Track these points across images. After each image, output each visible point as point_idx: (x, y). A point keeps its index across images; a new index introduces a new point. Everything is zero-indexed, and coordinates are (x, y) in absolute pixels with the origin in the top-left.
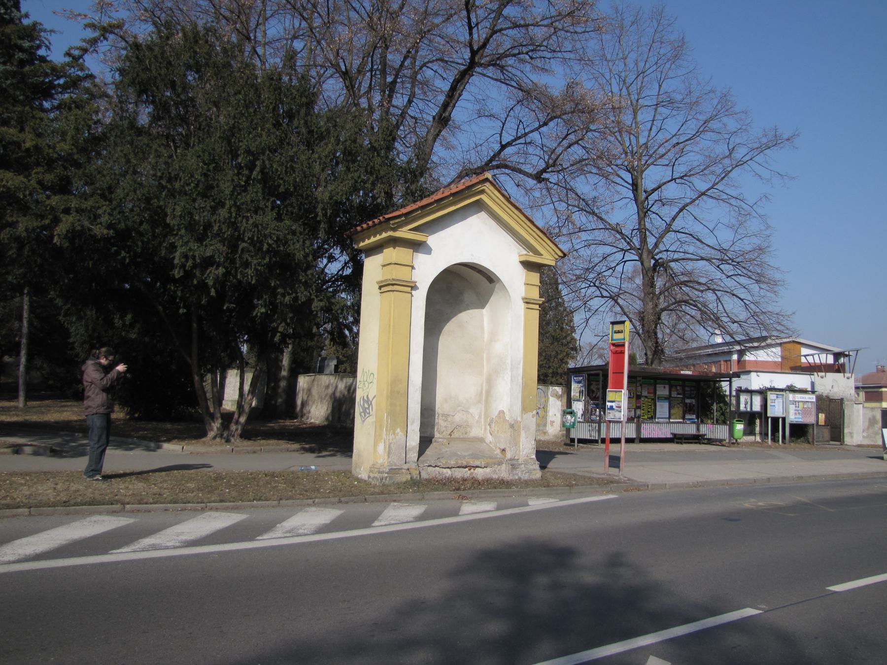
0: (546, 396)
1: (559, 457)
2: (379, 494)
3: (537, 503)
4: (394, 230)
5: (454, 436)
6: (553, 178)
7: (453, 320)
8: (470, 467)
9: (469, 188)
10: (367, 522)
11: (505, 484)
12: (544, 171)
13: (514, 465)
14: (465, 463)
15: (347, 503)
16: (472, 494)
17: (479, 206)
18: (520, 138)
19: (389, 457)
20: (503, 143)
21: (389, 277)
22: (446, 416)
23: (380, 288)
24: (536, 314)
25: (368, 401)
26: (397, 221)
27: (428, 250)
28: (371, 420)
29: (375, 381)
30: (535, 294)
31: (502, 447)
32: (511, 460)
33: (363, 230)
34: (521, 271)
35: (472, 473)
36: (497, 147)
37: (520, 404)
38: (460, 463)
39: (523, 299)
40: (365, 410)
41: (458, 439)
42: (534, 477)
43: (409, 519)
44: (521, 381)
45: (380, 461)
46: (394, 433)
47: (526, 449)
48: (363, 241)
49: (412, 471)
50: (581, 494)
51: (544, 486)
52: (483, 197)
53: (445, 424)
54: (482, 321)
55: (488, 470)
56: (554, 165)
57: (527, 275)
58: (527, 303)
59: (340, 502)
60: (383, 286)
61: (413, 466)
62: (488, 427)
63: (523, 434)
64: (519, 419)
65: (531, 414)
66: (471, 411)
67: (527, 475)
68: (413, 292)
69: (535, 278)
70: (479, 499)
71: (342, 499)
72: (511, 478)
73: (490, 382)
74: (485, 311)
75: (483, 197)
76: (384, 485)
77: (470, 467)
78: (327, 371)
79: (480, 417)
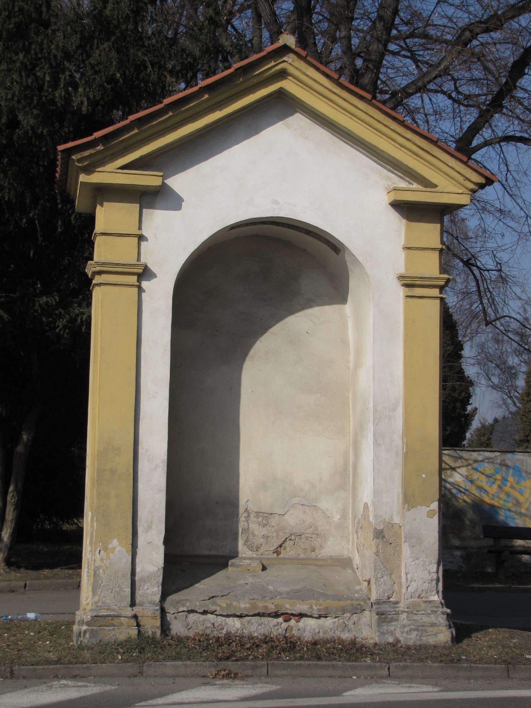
5: (289, 552)
10: (337, 693)
13: (385, 612)
14: (272, 608)
16: (254, 668)
17: (283, 105)
22: (265, 517)
26: (87, 153)
30: (430, 266)
32: (378, 602)
34: (395, 222)
38: (260, 606)
39: (401, 277)
41: (296, 561)
42: (432, 641)
46: (106, 549)
49: (143, 621)
52: (288, 85)
53: (264, 531)
55: (328, 622)
57: (408, 229)
63: (406, 550)
64: (397, 520)
65: (424, 510)
67: (414, 635)
68: (145, 284)
69: (430, 233)
72: (377, 640)
74: (348, 308)
77: (288, 616)
79: (344, 516)
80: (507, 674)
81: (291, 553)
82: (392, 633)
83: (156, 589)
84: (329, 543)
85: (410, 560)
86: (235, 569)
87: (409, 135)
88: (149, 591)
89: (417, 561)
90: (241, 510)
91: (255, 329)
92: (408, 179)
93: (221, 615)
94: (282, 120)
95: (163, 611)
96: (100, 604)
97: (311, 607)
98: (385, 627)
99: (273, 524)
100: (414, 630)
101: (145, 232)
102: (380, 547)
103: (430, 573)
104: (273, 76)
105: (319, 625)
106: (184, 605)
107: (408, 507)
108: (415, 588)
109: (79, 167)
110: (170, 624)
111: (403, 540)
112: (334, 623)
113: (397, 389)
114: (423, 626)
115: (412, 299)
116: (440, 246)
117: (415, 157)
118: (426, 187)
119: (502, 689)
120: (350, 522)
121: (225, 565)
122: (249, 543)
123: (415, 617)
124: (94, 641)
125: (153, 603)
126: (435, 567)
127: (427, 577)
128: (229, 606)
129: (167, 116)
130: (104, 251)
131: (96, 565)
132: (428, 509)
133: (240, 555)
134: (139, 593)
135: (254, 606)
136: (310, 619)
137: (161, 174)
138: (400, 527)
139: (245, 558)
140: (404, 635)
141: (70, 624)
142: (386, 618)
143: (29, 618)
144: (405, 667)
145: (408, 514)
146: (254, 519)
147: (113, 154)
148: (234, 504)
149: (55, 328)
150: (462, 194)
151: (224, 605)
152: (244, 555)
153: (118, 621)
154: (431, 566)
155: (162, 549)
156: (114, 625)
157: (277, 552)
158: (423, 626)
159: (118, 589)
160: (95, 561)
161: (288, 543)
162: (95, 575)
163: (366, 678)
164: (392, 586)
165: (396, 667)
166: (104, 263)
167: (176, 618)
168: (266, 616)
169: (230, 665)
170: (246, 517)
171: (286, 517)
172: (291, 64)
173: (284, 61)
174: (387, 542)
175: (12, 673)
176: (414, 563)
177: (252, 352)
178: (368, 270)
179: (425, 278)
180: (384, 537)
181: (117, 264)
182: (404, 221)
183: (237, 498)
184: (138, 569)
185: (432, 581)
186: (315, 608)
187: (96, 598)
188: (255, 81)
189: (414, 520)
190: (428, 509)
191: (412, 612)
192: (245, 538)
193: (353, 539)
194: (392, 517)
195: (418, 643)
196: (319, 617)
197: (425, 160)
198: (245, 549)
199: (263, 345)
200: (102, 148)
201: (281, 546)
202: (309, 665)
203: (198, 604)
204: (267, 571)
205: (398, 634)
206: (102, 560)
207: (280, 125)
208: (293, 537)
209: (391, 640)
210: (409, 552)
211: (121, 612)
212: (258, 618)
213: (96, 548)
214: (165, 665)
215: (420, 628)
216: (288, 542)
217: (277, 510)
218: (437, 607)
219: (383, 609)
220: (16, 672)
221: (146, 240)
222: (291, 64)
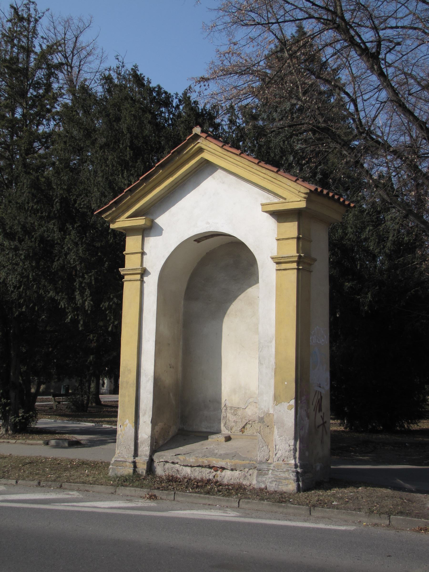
8: (216, 469)
14: (206, 463)
17: (206, 168)
22: (235, 410)
24: (292, 276)
26: (108, 213)
27: (159, 231)
30: (291, 249)
37: (272, 393)
39: (272, 258)
44: (273, 360)
49: (138, 465)
52: (205, 155)
53: (235, 418)
55: (236, 473)
57: (278, 227)
64: (271, 411)
69: (292, 228)
77: (216, 469)
80: (309, 512)
82: (264, 482)
83: (147, 448)
88: (144, 449)
89: (281, 438)
90: (223, 405)
91: (229, 298)
94: (211, 175)
95: (151, 462)
97: (227, 464)
100: (274, 481)
101: (145, 250)
104: (197, 151)
105: (232, 475)
106: (162, 458)
107: (276, 403)
108: (281, 455)
110: (155, 468)
115: (280, 271)
121: (206, 438)
122: (226, 425)
123: (276, 473)
125: (146, 455)
126: (292, 442)
127: (288, 448)
128: (185, 460)
130: (131, 262)
132: (288, 404)
137: (144, 217)
141: (108, 464)
146: (230, 411)
150: (300, 201)
154: (290, 441)
155: (150, 425)
156: (123, 466)
158: (280, 479)
161: (248, 426)
164: (269, 453)
167: (158, 465)
169: (156, 492)
171: (247, 410)
173: (199, 143)
174: (265, 425)
176: (279, 439)
179: (284, 257)
180: (264, 422)
185: (291, 450)
186: (229, 464)
188: (186, 157)
189: (280, 411)
190: (288, 404)
194: (268, 409)
199: (235, 307)
201: (244, 427)
207: (210, 179)
208: (250, 422)
209: (263, 486)
218: (291, 467)
219: (262, 467)
221: (146, 254)
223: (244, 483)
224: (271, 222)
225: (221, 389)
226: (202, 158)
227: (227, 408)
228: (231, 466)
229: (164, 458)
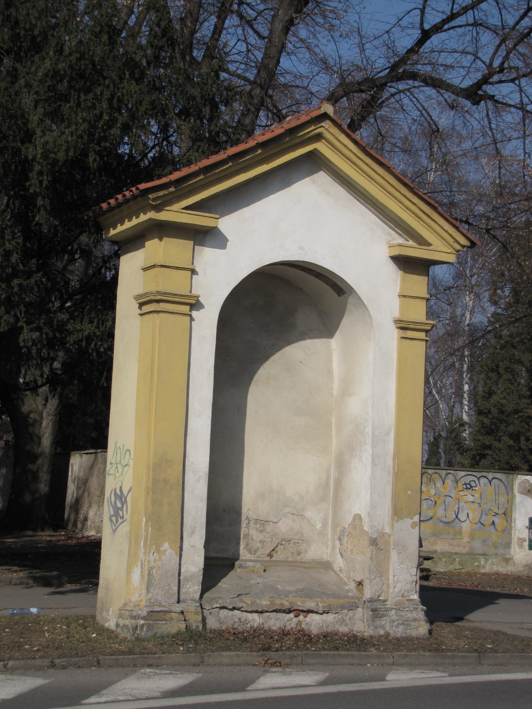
0: (509, 489)
1: (503, 603)
2: (124, 653)
3: (399, 678)
4: (158, 208)
5: (279, 556)
6: (504, 91)
7: (276, 357)
8: (298, 612)
9: (292, 131)
11: (355, 643)
12: (485, 80)
14: (287, 605)
15: (64, 667)
17: (314, 163)
18: (459, 14)
19: (148, 591)
20: (427, 27)
21: (152, 288)
22: (262, 523)
23: (141, 305)
25: (120, 496)
26: (161, 193)
28: (124, 528)
29: (131, 463)
30: (418, 313)
31: (358, 579)
32: (371, 601)
33: (111, 209)
34: (393, 275)
35: (300, 622)
36: (416, 34)
38: (278, 603)
39: (397, 321)
40: (116, 514)
41: (285, 563)
43: (152, 694)
44: (390, 463)
45: (135, 598)
46: (158, 551)
47: (401, 580)
48: (115, 228)
49: (189, 616)
50: (501, 667)
51: (429, 649)
52: (321, 147)
53: (261, 537)
54: (330, 360)
55: (330, 618)
56: (501, 70)
57: (403, 281)
58: (402, 328)
59: (53, 665)
60: (146, 302)
61: (191, 607)
62: (338, 543)
63: (394, 556)
64: (387, 530)
65: (409, 521)
66: (309, 514)
68: (194, 314)
69: (419, 284)
70: (303, 666)
71: (57, 661)
72: (371, 632)
73: (341, 465)
74: (334, 343)
75: (321, 147)
76: (138, 639)
77: (298, 612)
78: (481, 418)
79: (325, 525)
81: (281, 557)
82: (383, 627)
83: (196, 587)
84: (312, 547)
85: (397, 564)
86: (242, 570)
87: (416, 200)
88: (191, 590)
89: (402, 566)
90: (243, 517)
92: (406, 237)
93: (246, 611)
96: (153, 601)
97: (318, 605)
98: (378, 622)
99: (268, 530)
102: (374, 553)
103: (411, 576)
106: (217, 602)
109: (152, 205)
111: (392, 547)
112: (335, 618)
113: (390, 418)
114: (407, 621)
116: (428, 296)
117: (417, 219)
118: (420, 244)
119: (489, 673)
120: (329, 530)
121: (232, 567)
122: (248, 547)
124: (151, 634)
125: (193, 600)
127: (409, 579)
128: (253, 603)
129: (227, 166)
131: (150, 565)
132: (412, 521)
133: (241, 558)
134: (183, 590)
135: (273, 603)
136: (315, 614)
138: (390, 536)
139: (247, 561)
140: (394, 628)
142: (378, 614)
143: (32, 613)
144: (406, 656)
145: (396, 524)
146: (253, 526)
147: (180, 195)
148: (238, 513)
149: (66, 343)
151: (249, 602)
152: (244, 558)
153: (169, 616)
156: (165, 620)
157: (270, 555)
158: (407, 621)
159: (167, 587)
160: (149, 562)
162: (149, 574)
163: (378, 665)
165: (399, 655)
166: (165, 293)
167: (210, 613)
168: (281, 612)
170: (247, 524)
171: (279, 524)
172: (327, 129)
173: (322, 126)
175: (98, 662)
177: (256, 377)
178: (372, 313)
179: (417, 323)
180: (377, 544)
181: (176, 295)
182: (400, 273)
183: (240, 507)
184: (182, 571)
185: (412, 582)
186: (320, 605)
187: (150, 595)
188: (298, 141)
189: (401, 530)
190: (412, 521)
191: (399, 609)
192: (245, 542)
193: (48, 536)
195: (404, 635)
196: (324, 612)
197: (424, 222)
198: (246, 552)
199: (266, 371)
200: (174, 190)
201: (273, 550)
202: (334, 655)
203: (228, 601)
204: (267, 572)
205: (387, 628)
206: (155, 561)
207: (307, 180)
209: (382, 632)
210: (396, 558)
211: (171, 607)
212: (275, 613)
213: (150, 551)
214: (222, 655)
215: (406, 623)
216: (280, 546)
217: (271, 518)
219: (375, 607)
220: (101, 662)
222: (327, 129)
223: (341, 629)
224: (392, 268)
225: (241, 493)
226: (316, 149)
227: (249, 521)
228: (324, 608)
229: (220, 601)
